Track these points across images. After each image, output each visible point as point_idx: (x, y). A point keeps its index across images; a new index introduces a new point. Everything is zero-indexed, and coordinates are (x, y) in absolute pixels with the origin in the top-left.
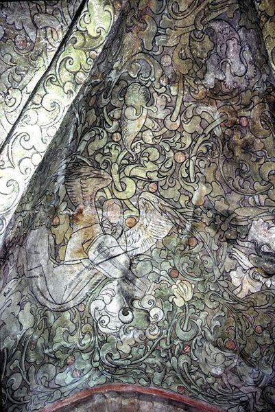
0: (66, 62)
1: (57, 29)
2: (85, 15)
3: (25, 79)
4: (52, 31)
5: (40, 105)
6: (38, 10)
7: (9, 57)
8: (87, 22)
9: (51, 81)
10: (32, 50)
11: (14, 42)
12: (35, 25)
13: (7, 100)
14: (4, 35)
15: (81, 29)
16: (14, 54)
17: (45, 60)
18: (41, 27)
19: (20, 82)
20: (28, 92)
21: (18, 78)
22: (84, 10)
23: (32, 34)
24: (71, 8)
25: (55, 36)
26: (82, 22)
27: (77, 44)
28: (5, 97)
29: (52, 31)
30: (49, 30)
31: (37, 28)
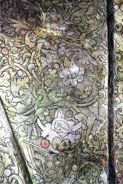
0: (119, 69)
1: (103, 54)
2: (116, 44)
3: (102, 83)
4: (102, 57)
5: (118, 94)
6: (91, 51)
7: (91, 78)
8: (118, 47)
9: (117, 81)
10: (98, 69)
11: (90, 71)
12: (94, 58)
13: (100, 96)
14: (85, 70)
15: (118, 51)
16: (92, 76)
17: (106, 70)
18: (96, 58)
19: (100, 86)
20: (106, 87)
21: (99, 84)
22: (114, 43)
23: (94, 63)
24: (104, 42)
25: (104, 58)
26: (117, 48)
27: (119, 59)
28: (99, 95)
29: (102, 57)
30: (100, 57)
31: (95, 59)
